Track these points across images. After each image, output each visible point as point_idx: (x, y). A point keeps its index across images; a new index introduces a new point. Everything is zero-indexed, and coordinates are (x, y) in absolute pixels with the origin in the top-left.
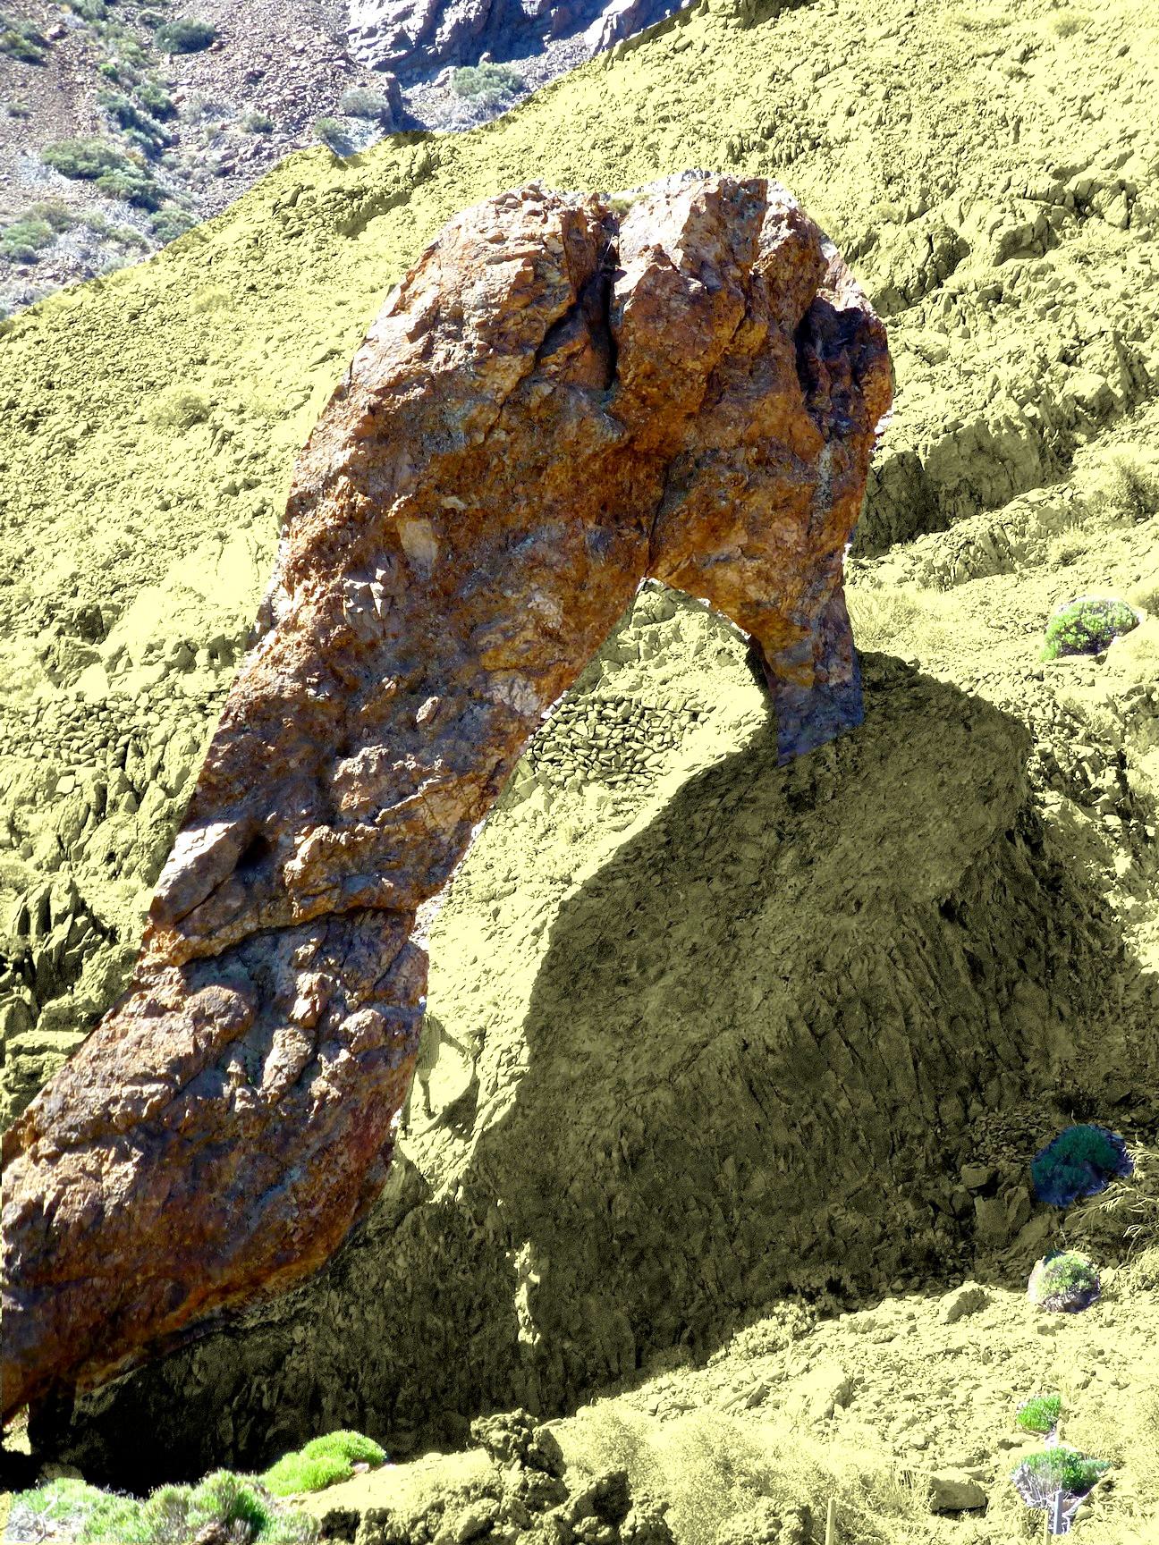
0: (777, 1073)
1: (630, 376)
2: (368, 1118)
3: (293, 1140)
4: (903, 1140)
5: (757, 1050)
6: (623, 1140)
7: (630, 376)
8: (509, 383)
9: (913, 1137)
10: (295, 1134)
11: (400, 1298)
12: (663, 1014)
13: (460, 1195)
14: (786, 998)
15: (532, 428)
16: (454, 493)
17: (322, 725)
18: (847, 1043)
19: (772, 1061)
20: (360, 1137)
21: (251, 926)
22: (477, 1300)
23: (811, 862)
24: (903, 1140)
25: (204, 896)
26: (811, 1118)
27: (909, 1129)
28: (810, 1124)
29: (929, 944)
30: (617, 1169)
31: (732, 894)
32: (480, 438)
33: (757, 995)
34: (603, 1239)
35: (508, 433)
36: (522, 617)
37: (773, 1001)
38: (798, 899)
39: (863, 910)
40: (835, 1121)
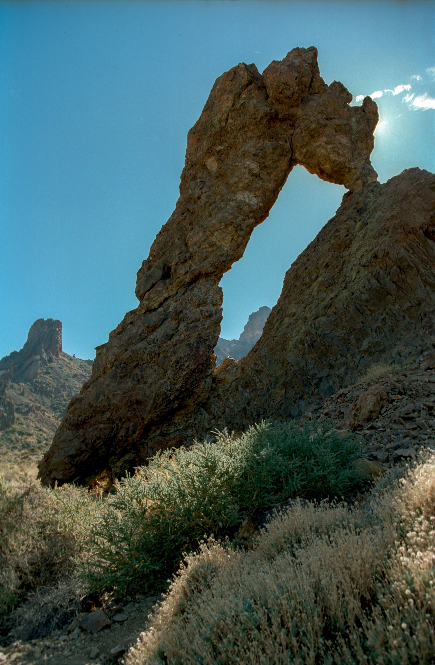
0: (367, 301)
1: (271, 93)
2: (197, 347)
3: (167, 360)
4: (425, 315)
5: (357, 294)
6: (307, 338)
7: (271, 93)
8: (230, 104)
9: (429, 312)
10: (167, 357)
11: (232, 414)
12: (319, 291)
13: (58, 329)
14: (366, 273)
15: (240, 116)
16: (220, 145)
17: (185, 226)
18: (394, 282)
19: (364, 297)
20: (194, 355)
21: (166, 295)
22: (262, 411)
23: (367, 224)
24: (425, 315)
25: (149, 288)
26: (384, 315)
27: (427, 309)
28: (385, 318)
29: (421, 244)
30: (307, 350)
31: (339, 242)
32: (223, 124)
33: (354, 274)
34: (304, 377)
35: (232, 119)
36: (243, 170)
37: (361, 275)
38: (364, 237)
39: (390, 232)
40: (395, 314)
